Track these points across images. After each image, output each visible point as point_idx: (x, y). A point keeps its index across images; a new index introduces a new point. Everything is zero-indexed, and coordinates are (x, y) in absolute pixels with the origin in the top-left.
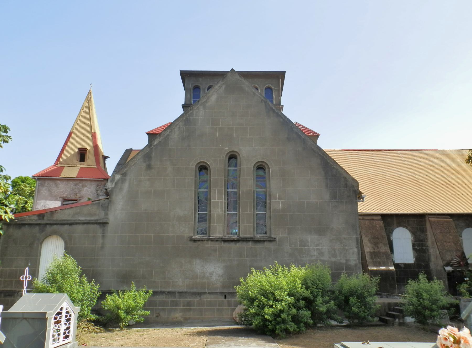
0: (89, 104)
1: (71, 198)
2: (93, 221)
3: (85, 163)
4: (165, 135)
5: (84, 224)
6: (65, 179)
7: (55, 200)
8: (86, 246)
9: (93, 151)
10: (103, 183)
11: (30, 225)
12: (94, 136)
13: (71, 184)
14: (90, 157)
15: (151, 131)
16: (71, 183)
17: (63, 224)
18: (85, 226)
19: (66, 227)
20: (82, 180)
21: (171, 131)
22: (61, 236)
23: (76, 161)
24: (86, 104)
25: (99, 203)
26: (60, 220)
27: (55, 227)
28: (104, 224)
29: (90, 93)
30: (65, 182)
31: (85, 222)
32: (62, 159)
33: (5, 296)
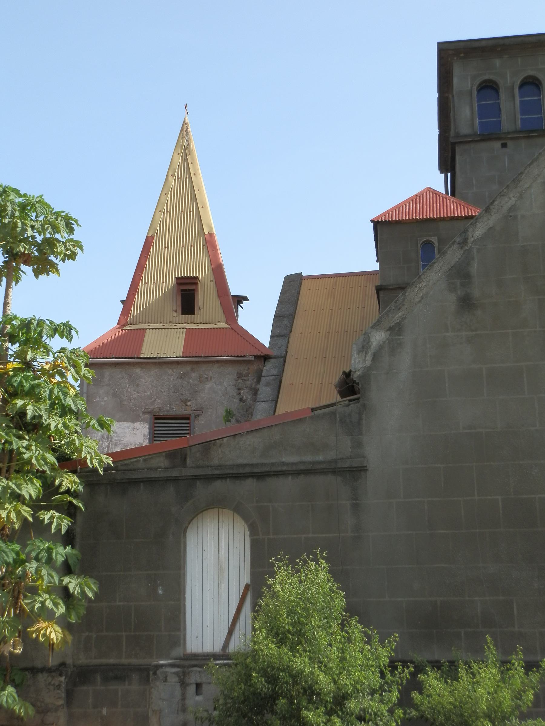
0: (186, 160)
1: (172, 413)
2: (323, 466)
3: (197, 317)
4: (505, 208)
5: (297, 473)
6: (155, 363)
7: (134, 421)
8: (310, 535)
9: (213, 284)
10: (255, 367)
11: (150, 482)
12: (210, 243)
13: (171, 376)
14: (206, 298)
15: (384, 214)
16: (170, 372)
17: (238, 475)
18: (302, 480)
19: (250, 483)
20: (197, 362)
21: (521, 197)
22: (239, 510)
23: (172, 311)
24: (178, 160)
25: (333, 413)
26: (232, 467)
27: (218, 484)
28: (353, 472)
29: (184, 129)
30: (155, 371)
31: (302, 467)
32: (135, 310)
33: (106, 680)
